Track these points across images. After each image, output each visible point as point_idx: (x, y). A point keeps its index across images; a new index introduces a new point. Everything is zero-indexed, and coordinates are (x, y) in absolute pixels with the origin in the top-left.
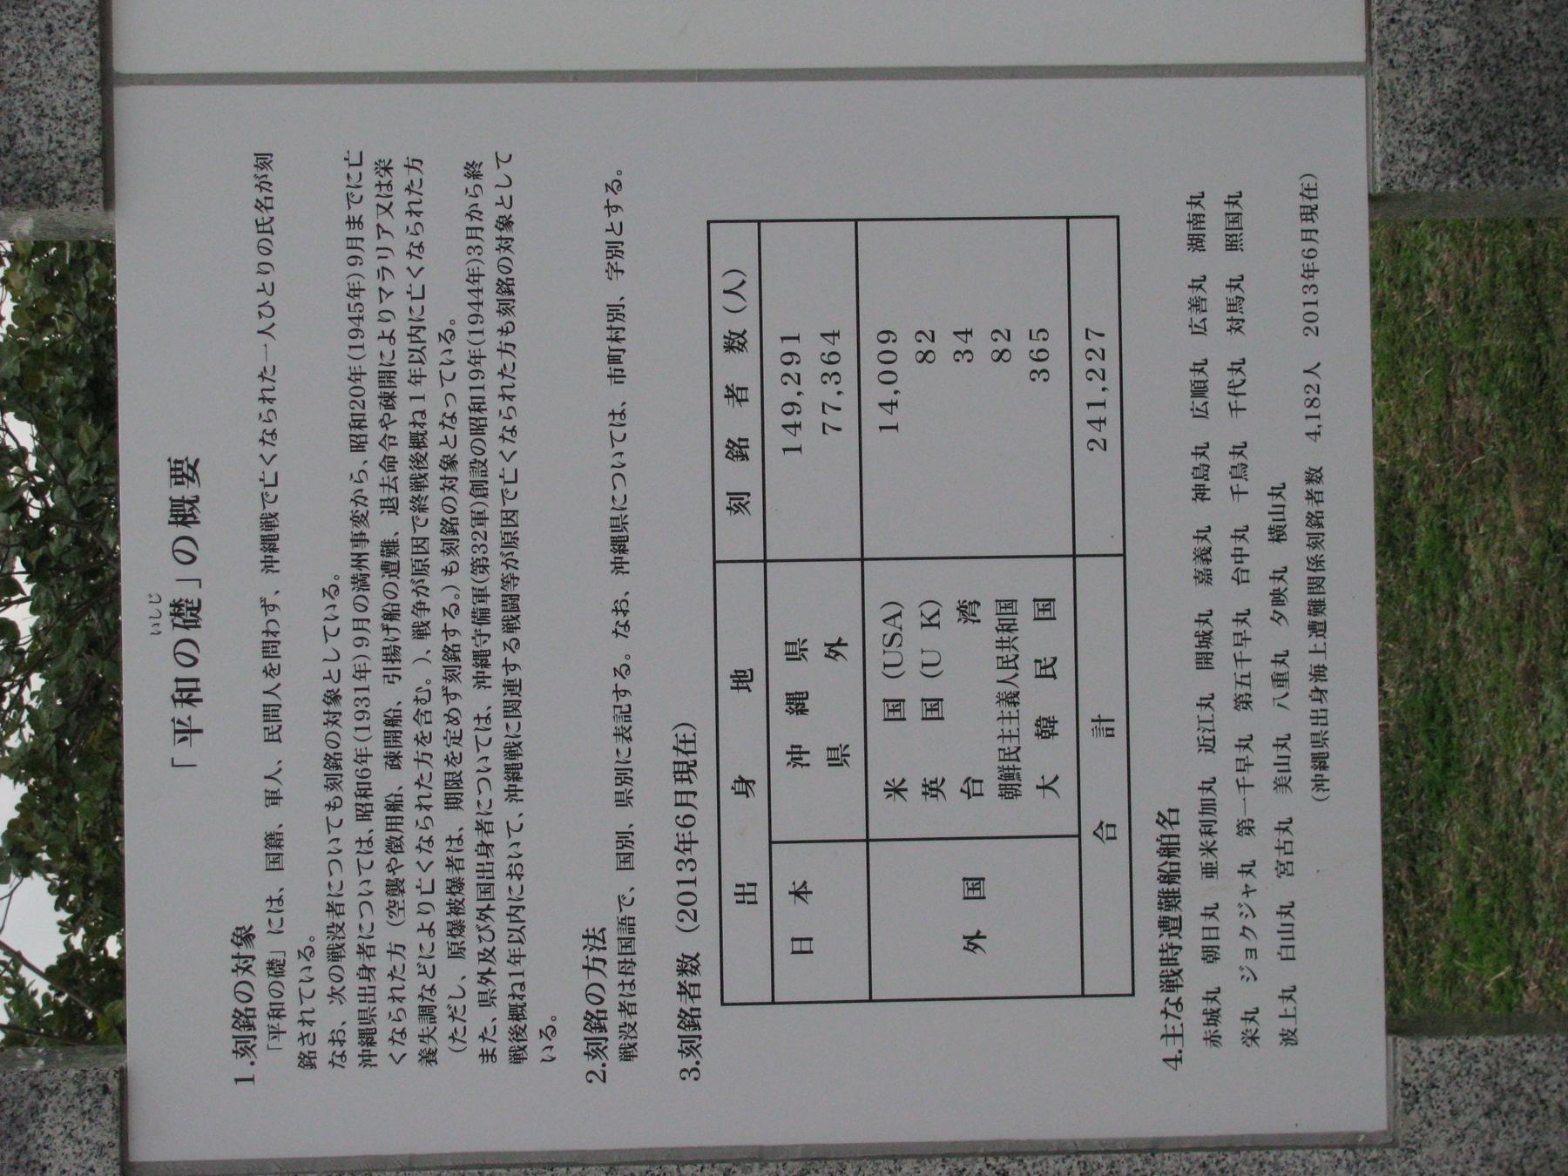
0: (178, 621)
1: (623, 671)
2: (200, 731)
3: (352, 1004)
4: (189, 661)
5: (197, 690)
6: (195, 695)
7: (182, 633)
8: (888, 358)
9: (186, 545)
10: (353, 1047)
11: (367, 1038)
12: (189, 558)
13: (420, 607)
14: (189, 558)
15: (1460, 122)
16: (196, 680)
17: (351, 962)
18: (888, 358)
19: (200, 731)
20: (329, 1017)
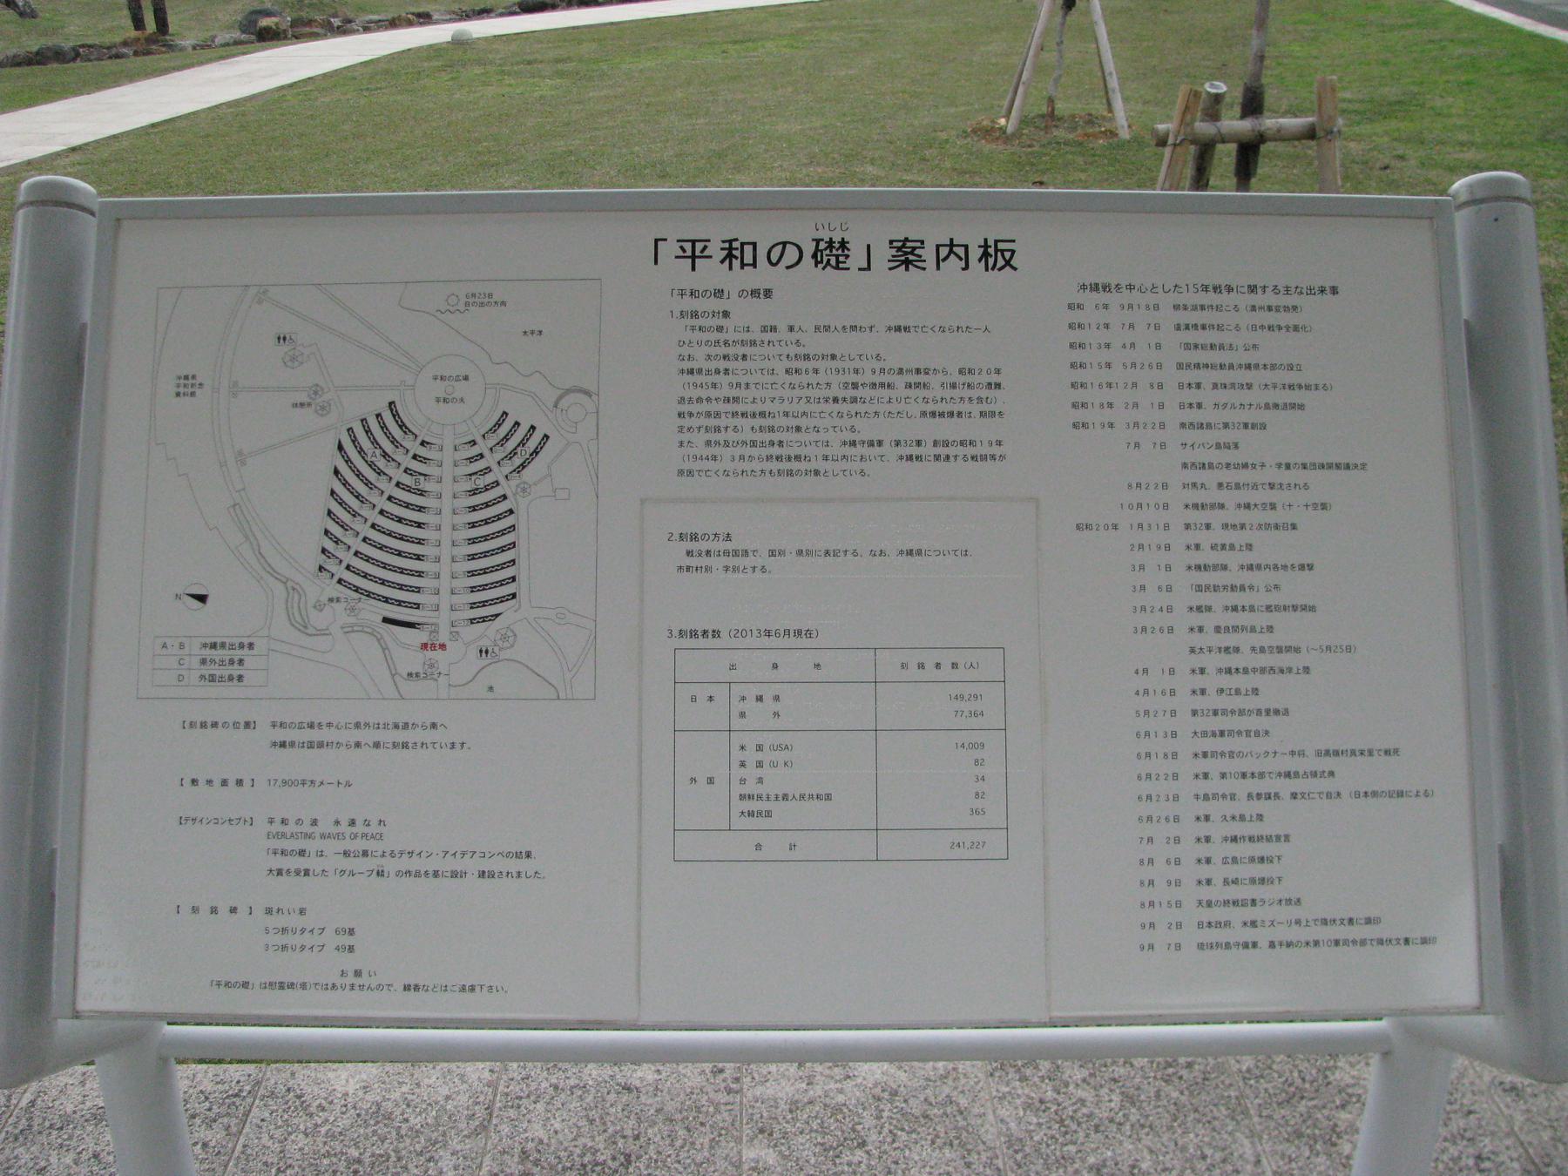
0: (822, 245)
1: (855, 553)
2: (693, 269)
3: (705, 365)
4: (774, 258)
5: (743, 265)
6: (736, 263)
7: (809, 249)
8: (973, 746)
9: (791, 255)
10: (687, 365)
11: (691, 372)
12: (774, 260)
13: (691, 415)
14: (774, 260)
15: (1091, 1075)
16: (754, 265)
17: (722, 365)
18: (973, 746)
19: (693, 269)
20: (700, 353)
